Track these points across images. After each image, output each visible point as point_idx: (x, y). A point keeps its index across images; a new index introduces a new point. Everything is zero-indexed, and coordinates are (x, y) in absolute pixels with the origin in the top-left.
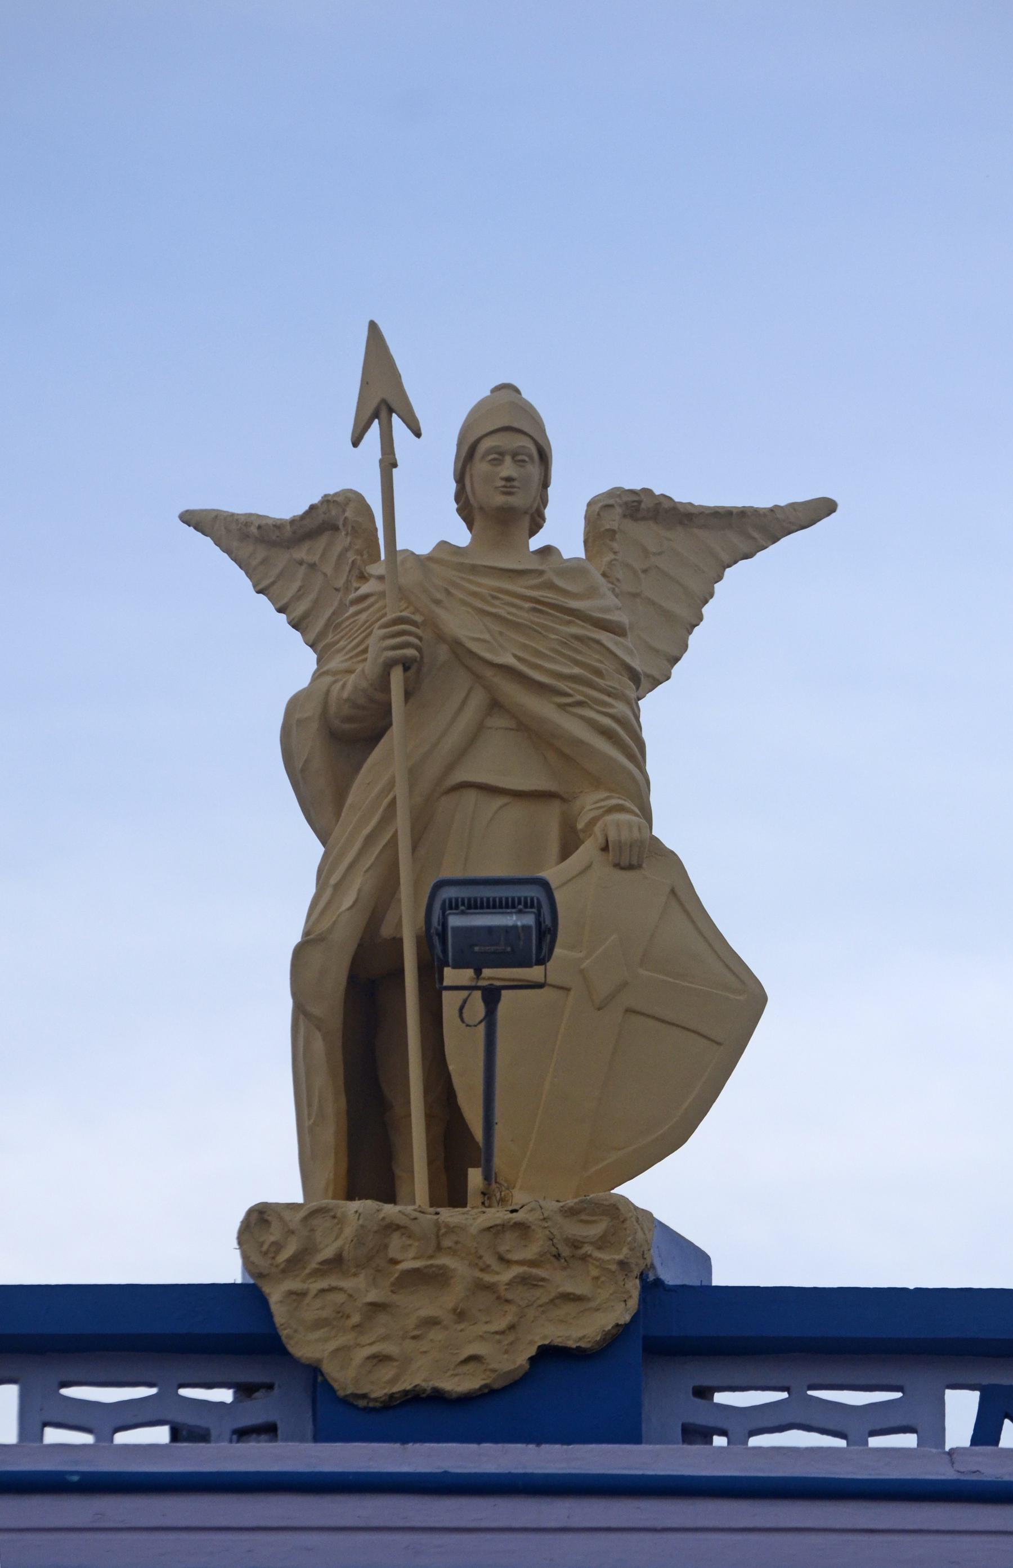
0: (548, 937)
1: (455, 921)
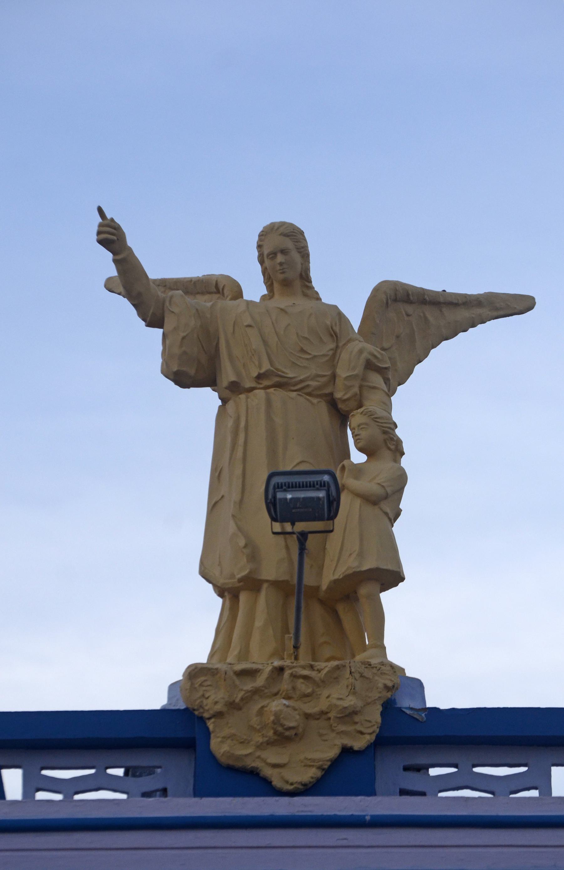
0: (335, 503)
1: (280, 495)
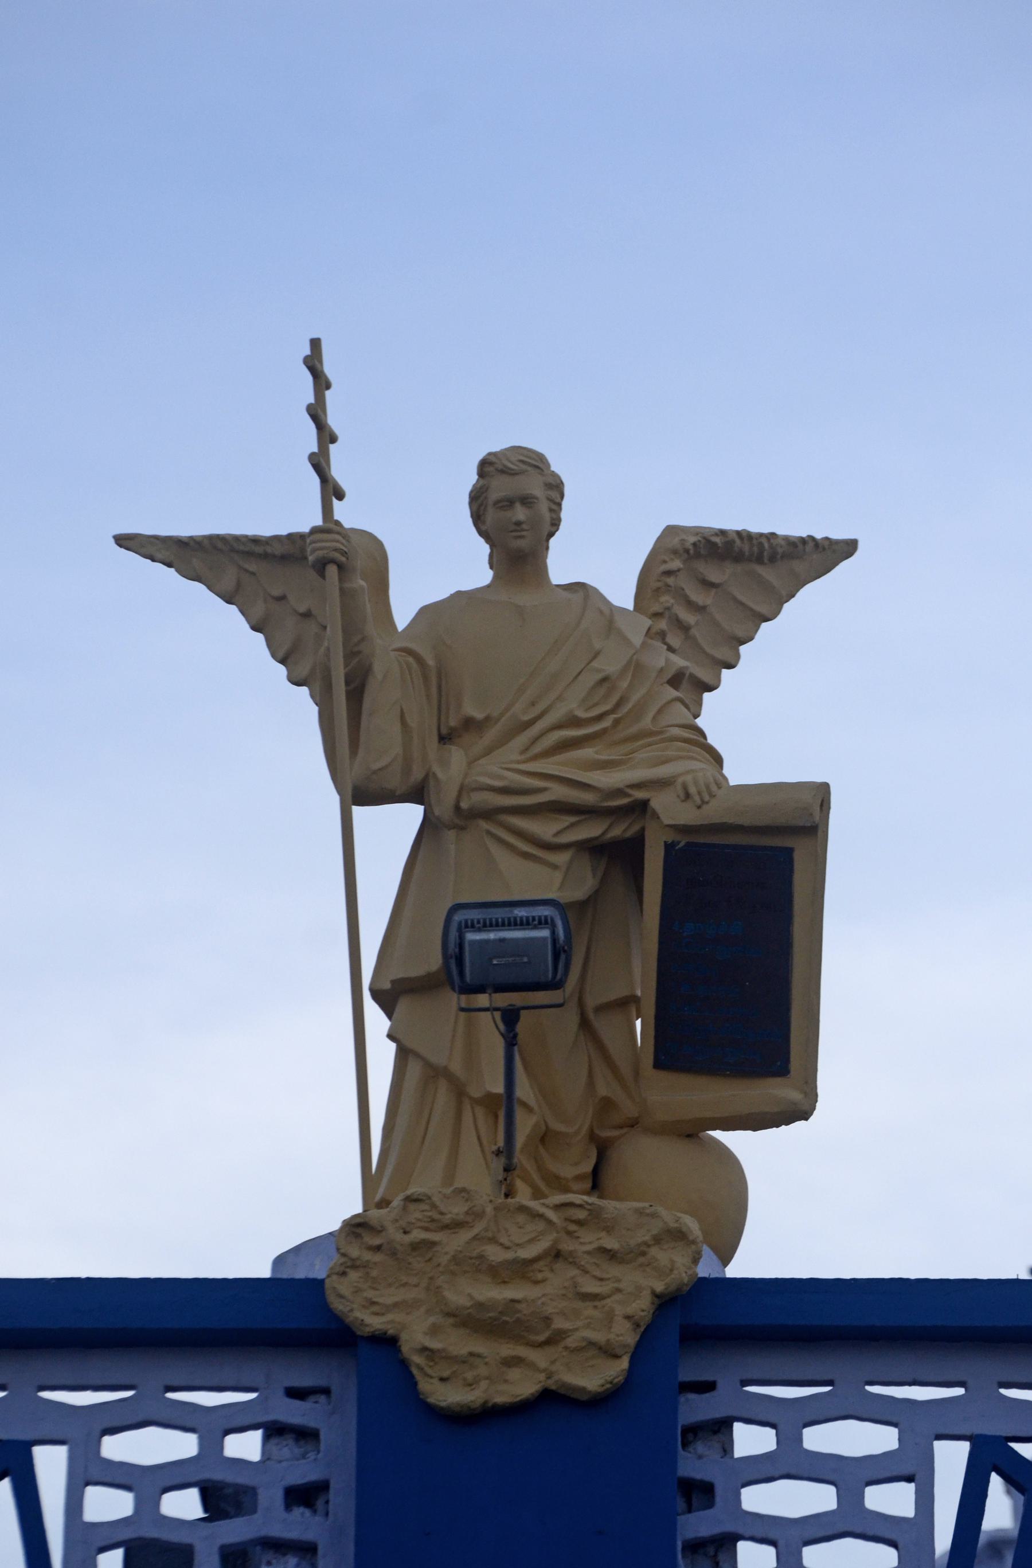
1: (471, 936)
